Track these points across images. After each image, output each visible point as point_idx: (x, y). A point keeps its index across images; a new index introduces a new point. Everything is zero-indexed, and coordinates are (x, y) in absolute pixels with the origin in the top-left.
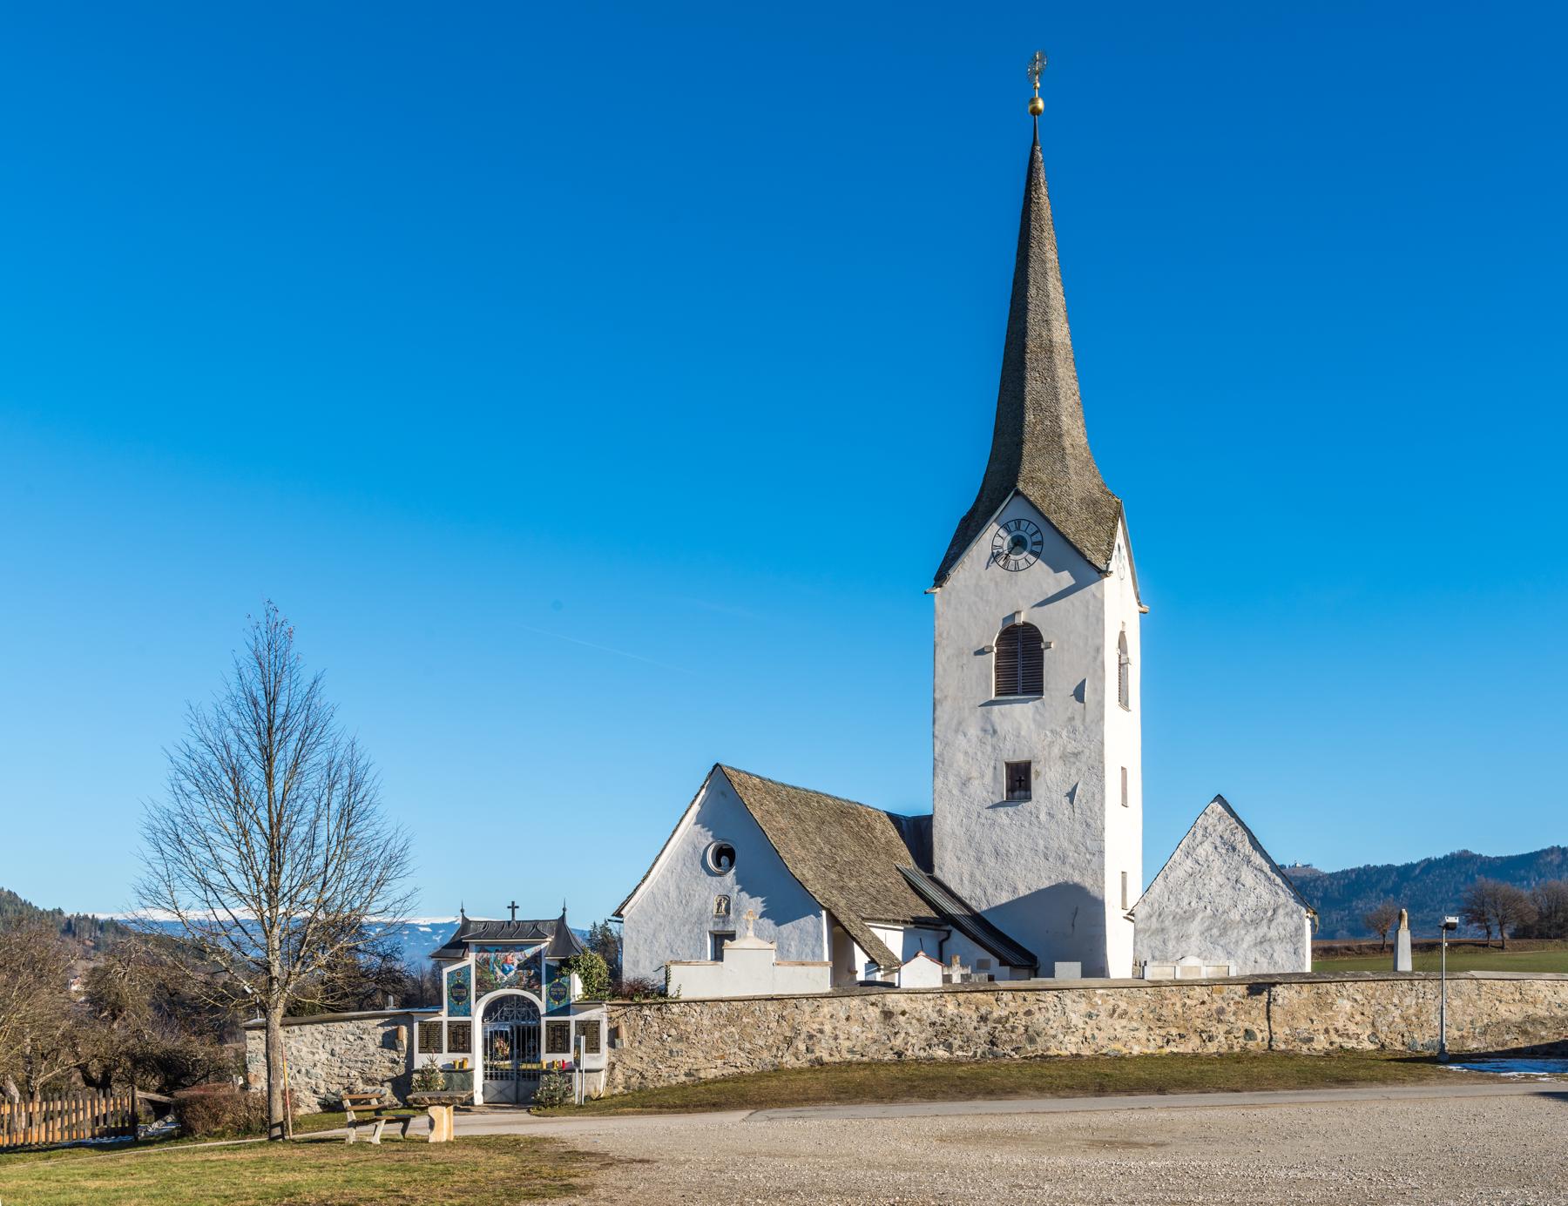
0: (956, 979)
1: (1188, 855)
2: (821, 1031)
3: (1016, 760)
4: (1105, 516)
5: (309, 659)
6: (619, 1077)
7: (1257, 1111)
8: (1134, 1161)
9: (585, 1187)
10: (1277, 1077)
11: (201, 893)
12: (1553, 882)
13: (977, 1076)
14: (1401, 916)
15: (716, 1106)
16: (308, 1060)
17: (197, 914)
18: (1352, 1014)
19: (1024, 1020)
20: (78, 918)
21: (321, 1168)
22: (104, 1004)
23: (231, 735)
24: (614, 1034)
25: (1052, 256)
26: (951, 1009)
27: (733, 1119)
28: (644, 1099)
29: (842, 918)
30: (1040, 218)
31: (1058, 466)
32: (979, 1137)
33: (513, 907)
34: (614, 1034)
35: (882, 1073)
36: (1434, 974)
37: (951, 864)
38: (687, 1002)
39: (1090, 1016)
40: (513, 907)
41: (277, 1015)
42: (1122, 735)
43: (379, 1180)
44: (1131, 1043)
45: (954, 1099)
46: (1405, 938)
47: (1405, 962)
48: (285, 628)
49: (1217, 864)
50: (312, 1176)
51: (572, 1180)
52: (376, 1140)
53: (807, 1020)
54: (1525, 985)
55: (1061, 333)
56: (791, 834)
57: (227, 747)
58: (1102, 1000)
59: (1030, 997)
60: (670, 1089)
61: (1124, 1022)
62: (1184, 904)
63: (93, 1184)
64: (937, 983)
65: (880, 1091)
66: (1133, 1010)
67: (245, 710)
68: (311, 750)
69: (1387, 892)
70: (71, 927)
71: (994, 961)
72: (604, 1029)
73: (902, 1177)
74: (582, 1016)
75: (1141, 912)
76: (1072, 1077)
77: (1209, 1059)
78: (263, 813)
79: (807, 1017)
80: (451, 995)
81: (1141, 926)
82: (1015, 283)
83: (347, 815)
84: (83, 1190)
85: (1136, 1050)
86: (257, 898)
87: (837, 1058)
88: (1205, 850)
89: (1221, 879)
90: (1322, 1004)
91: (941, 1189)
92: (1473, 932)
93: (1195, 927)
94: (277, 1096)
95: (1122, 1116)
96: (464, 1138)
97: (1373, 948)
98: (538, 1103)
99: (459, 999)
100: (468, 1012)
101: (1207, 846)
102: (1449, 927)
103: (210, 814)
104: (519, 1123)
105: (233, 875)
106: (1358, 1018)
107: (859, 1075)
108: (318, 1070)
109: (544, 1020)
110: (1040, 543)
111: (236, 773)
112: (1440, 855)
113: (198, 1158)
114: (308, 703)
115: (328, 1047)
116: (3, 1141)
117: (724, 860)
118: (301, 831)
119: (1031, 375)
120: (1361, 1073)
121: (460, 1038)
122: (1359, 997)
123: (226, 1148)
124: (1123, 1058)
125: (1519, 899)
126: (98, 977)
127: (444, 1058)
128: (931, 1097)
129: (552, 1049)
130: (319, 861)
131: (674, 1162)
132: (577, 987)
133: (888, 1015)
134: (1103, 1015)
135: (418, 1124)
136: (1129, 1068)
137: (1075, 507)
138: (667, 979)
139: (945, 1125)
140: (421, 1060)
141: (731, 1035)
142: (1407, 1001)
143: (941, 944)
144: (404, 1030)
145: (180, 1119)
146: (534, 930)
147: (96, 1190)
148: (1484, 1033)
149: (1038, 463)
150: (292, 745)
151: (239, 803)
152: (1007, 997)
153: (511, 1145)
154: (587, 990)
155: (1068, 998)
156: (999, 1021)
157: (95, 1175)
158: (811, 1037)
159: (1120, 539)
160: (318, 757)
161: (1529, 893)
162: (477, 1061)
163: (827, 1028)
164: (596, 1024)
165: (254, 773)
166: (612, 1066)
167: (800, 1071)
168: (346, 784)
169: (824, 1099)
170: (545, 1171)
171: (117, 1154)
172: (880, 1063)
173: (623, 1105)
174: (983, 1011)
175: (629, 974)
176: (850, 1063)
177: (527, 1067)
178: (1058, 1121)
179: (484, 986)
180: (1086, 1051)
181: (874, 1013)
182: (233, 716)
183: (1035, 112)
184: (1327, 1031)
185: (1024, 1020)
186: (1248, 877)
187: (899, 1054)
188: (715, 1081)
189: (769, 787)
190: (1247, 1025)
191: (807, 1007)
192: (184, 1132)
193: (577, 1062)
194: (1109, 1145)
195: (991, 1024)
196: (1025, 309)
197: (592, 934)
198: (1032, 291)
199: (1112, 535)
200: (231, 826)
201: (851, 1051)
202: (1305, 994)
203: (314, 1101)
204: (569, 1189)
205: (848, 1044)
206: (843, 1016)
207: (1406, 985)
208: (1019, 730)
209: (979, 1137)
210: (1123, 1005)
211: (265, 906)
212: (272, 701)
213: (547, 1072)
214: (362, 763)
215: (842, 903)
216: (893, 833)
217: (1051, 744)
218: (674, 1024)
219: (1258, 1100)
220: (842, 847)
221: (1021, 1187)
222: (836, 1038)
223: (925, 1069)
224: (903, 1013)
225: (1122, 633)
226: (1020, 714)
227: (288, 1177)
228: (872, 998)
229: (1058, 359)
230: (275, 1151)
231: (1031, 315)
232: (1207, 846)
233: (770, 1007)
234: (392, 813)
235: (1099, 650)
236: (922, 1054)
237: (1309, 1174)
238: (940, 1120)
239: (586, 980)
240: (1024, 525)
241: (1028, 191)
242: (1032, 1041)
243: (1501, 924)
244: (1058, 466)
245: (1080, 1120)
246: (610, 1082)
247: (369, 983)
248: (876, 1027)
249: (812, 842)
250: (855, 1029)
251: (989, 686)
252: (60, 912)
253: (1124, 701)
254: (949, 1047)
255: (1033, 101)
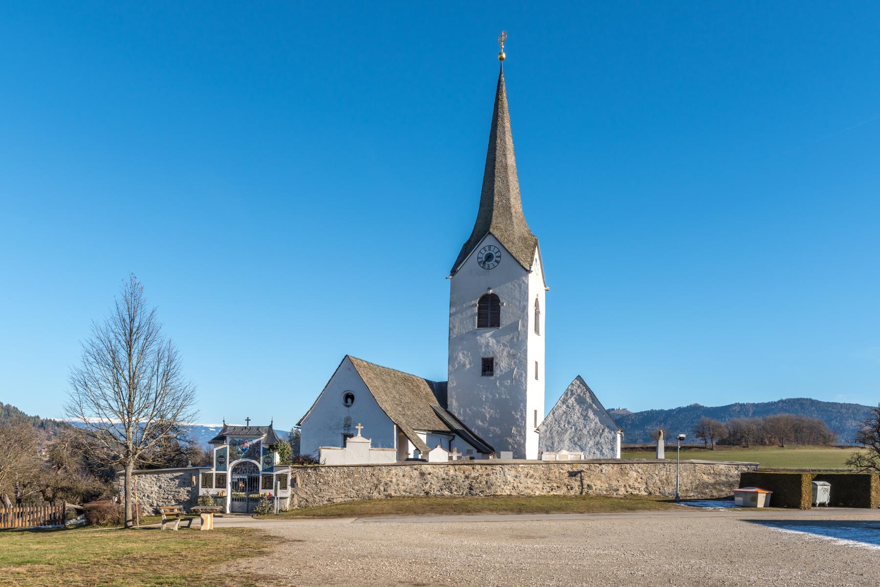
0: (455, 458)
1: (563, 403)
2: (391, 482)
3: (486, 357)
4: (530, 245)
5: (150, 301)
6: (296, 502)
7: (590, 523)
8: (528, 545)
9: (269, 553)
10: (601, 507)
11: (96, 410)
12: (736, 419)
13: (463, 504)
14: (660, 433)
15: (340, 516)
16: (145, 490)
17: (95, 420)
18: (636, 479)
19: (486, 478)
20: (47, 420)
21: (146, 541)
22: (56, 462)
23: (112, 335)
24: (294, 481)
25: (508, 125)
26: (452, 472)
27: (347, 522)
28: (306, 512)
29: (403, 429)
30: (502, 107)
31: (509, 222)
32: (460, 532)
33: (248, 420)
34: (294, 481)
35: (419, 502)
36: (675, 461)
37: (453, 404)
38: (329, 467)
39: (516, 477)
40: (248, 420)
41: (131, 469)
42: (536, 347)
43: (172, 547)
44: (535, 490)
45: (451, 514)
46: (661, 444)
47: (661, 455)
48: (140, 286)
49: (578, 407)
50: (141, 545)
51: (264, 549)
52: (176, 528)
53: (385, 477)
54: (716, 467)
55: (511, 160)
56: (381, 389)
57: (110, 343)
58: (523, 470)
59: (489, 467)
60: (320, 507)
61: (532, 480)
62: (562, 426)
63: (36, 547)
64: (446, 460)
65: (417, 510)
66: (536, 475)
67: (119, 324)
68: (151, 344)
69: (660, 422)
70: (43, 425)
71: (475, 451)
72: (290, 478)
73: (418, 550)
74: (279, 472)
75: (543, 429)
76: (507, 505)
77: (571, 498)
78: (126, 373)
79: (385, 475)
80: (217, 461)
81: (542, 435)
82: (491, 137)
83: (167, 375)
84: (30, 550)
85: (537, 493)
86: (122, 413)
87: (398, 494)
88: (572, 401)
89: (579, 414)
90: (623, 473)
91: (435, 556)
92: (699, 442)
93: (567, 437)
94: (130, 505)
95: (527, 523)
96: (218, 529)
97: (642, 448)
98: (257, 513)
99: (221, 463)
100: (225, 469)
101: (573, 399)
102: (681, 439)
103: (100, 372)
104: (247, 522)
105: (111, 402)
106: (639, 480)
107: (408, 502)
108: (153, 495)
109: (261, 473)
110: (500, 257)
111: (114, 353)
112: (685, 406)
113: (89, 535)
114: (149, 322)
115: (158, 484)
116: (1, 526)
117: (349, 400)
118: (145, 382)
119: (497, 179)
120: (640, 506)
121: (221, 482)
122: (640, 470)
123: (104, 531)
124: (531, 497)
125: (720, 427)
126: (53, 449)
127: (213, 491)
128: (441, 513)
129: (264, 488)
130: (153, 396)
131: (315, 542)
132: (277, 458)
133: (422, 474)
134: (522, 476)
135: (196, 522)
136: (533, 501)
137: (516, 241)
138: (319, 455)
139: (445, 526)
140: (202, 491)
141: (349, 482)
142: (662, 473)
143: (450, 442)
144: (194, 478)
145: (86, 517)
146: (258, 431)
147: (37, 550)
148: (696, 488)
149: (500, 219)
150: (141, 341)
151: (116, 367)
152: (478, 467)
153: (240, 532)
154: (282, 460)
155: (506, 468)
156: (474, 478)
157: (39, 543)
158: (386, 484)
159: (536, 256)
160: (154, 347)
161: (725, 425)
162: (228, 492)
163: (394, 480)
164: (286, 476)
165: (123, 355)
166: (293, 496)
167: (381, 500)
168: (166, 360)
169: (391, 513)
170: (253, 544)
171: (50, 534)
172: (418, 497)
173: (297, 514)
174: (467, 473)
175: (303, 452)
176: (404, 497)
177: (252, 497)
178: (498, 525)
179: (233, 457)
180: (514, 493)
181: (416, 473)
182: (114, 327)
183: (501, 59)
184: (625, 486)
185: (486, 478)
186: (591, 415)
187: (427, 493)
188: (341, 504)
189: (371, 366)
190: (589, 483)
191: (384, 470)
192: (89, 523)
193: (276, 494)
194: (519, 537)
195: (470, 480)
196: (495, 149)
197: (291, 433)
198: (498, 141)
199: (533, 254)
200: (111, 378)
201: (405, 491)
202: (615, 469)
203: (151, 509)
204: (261, 553)
205: (403, 488)
206: (401, 474)
207: (661, 465)
208: (488, 343)
209: (460, 532)
210: (532, 472)
211: (126, 417)
212: (132, 320)
213: (262, 498)
214: (174, 351)
215: (404, 422)
216: (429, 390)
217: (503, 350)
218: (322, 476)
219: (590, 517)
220: (405, 395)
221: (472, 556)
222: (398, 485)
223: (439, 500)
224: (430, 474)
225: (537, 299)
226: (487, 337)
227: (130, 545)
228: (415, 467)
229: (510, 172)
230: (126, 533)
231: (497, 152)
232: (573, 399)
233: (368, 469)
234: (187, 374)
235: (525, 308)
236: (438, 493)
237: (606, 552)
238: (443, 524)
239: (282, 455)
240: (492, 248)
241: (497, 95)
242: (489, 488)
243: (712, 438)
244: (509, 222)
245: (508, 525)
246: (292, 504)
247: (173, 455)
248: (417, 480)
249: (391, 393)
250: (407, 481)
251: (474, 322)
252: (38, 417)
253: (537, 330)
254: (451, 491)
255: (500, 54)
